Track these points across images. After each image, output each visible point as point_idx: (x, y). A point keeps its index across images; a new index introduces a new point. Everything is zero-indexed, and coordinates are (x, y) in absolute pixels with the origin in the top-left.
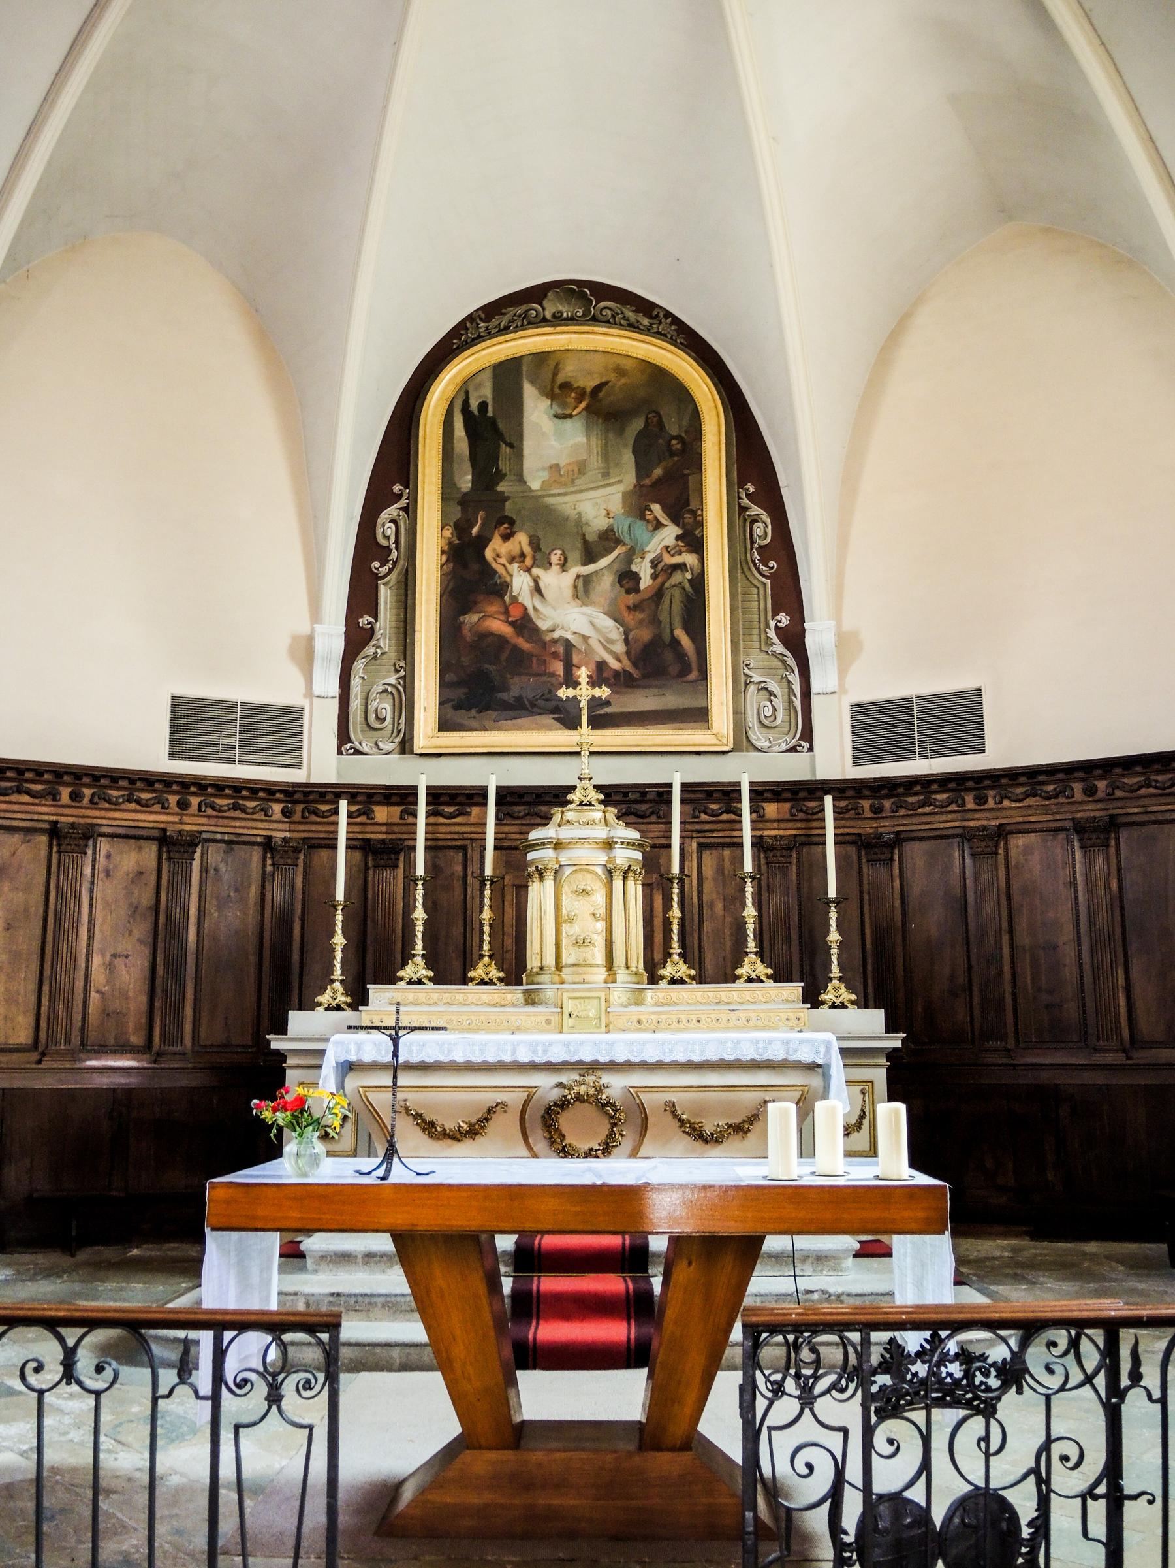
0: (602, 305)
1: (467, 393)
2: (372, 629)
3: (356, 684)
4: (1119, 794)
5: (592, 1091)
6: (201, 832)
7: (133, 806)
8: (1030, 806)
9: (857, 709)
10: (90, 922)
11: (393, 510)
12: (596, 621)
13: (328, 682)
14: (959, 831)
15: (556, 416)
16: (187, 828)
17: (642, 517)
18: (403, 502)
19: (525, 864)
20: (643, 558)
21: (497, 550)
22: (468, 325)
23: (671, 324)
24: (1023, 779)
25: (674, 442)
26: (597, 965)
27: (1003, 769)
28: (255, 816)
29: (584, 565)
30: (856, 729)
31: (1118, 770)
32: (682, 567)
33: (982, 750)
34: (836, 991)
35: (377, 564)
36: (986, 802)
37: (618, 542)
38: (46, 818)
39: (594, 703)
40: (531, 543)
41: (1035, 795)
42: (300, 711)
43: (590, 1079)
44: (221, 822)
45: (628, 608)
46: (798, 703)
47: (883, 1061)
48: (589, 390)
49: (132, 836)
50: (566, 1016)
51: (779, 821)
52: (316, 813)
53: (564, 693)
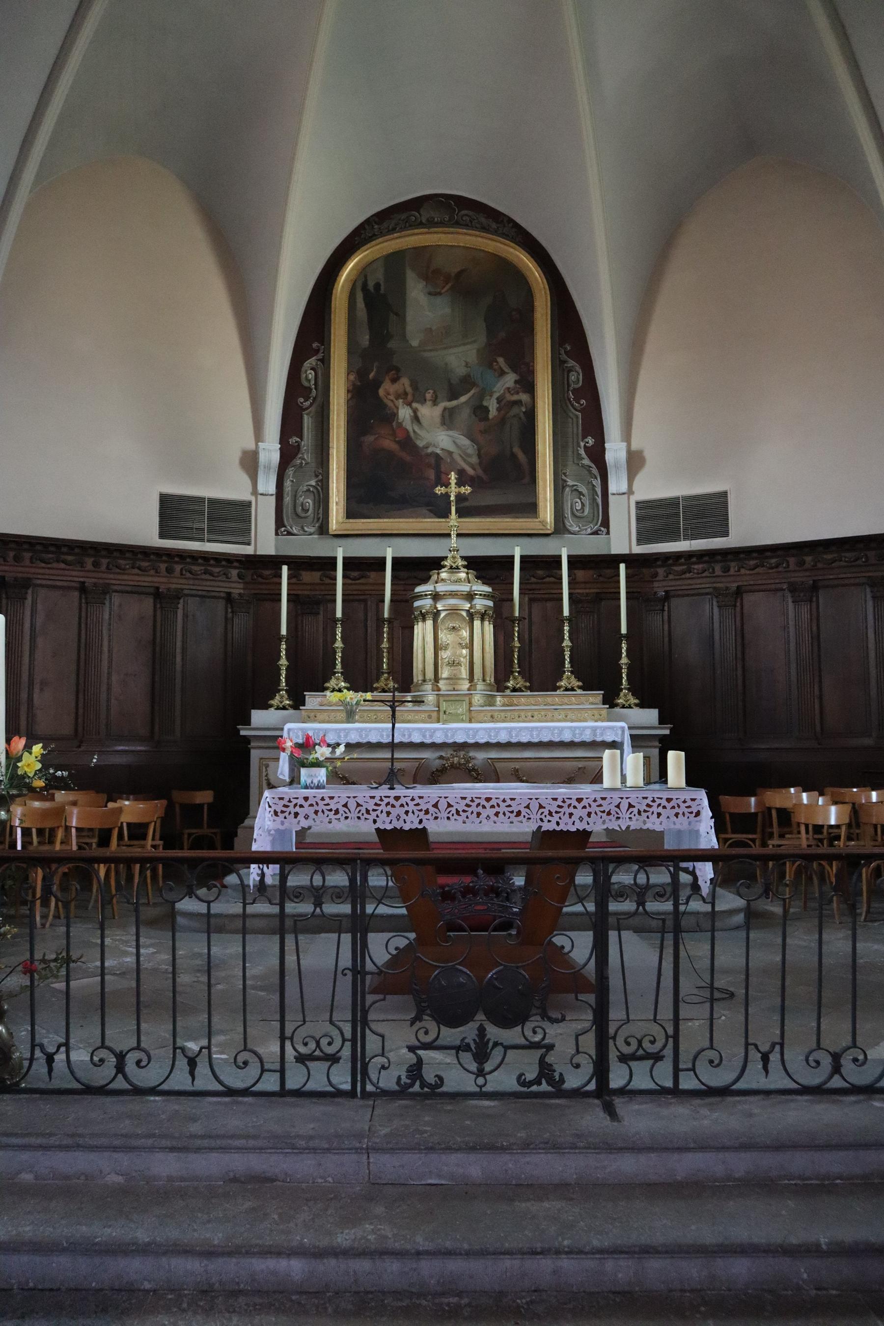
0: (463, 212)
1: (366, 277)
2: (299, 446)
3: (288, 484)
4: (820, 565)
5: (462, 761)
6: (182, 590)
7: (136, 571)
8: (758, 574)
9: (641, 506)
10: (109, 651)
11: (312, 361)
12: (457, 441)
13: (268, 484)
14: (711, 590)
15: (430, 294)
16: (174, 586)
17: (490, 366)
18: (320, 356)
19: (412, 609)
20: (491, 396)
21: (387, 390)
22: (366, 226)
23: (512, 227)
24: (755, 555)
25: (514, 313)
26: (463, 679)
27: (740, 548)
28: (220, 578)
29: (450, 400)
30: (639, 519)
31: (821, 549)
32: (519, 403)
33: (726, 534)
34: (625, 696)
35: (302, 400)
36: (729, 570)
37: (474, 385)
38: (77, 579)
39: (460, 498)
40: (411, 385)
41: (763, 566)
42: (249, 504)
43: (462, 754)
44: (197, 582)
45: (481, 431)
46: (599, 500)
47: (657, 744)
48: (453, 275)
49: (137, 591)
50: (442, 713)
51: (585, 583)
52: (261, 576)
53: (439, 490)
